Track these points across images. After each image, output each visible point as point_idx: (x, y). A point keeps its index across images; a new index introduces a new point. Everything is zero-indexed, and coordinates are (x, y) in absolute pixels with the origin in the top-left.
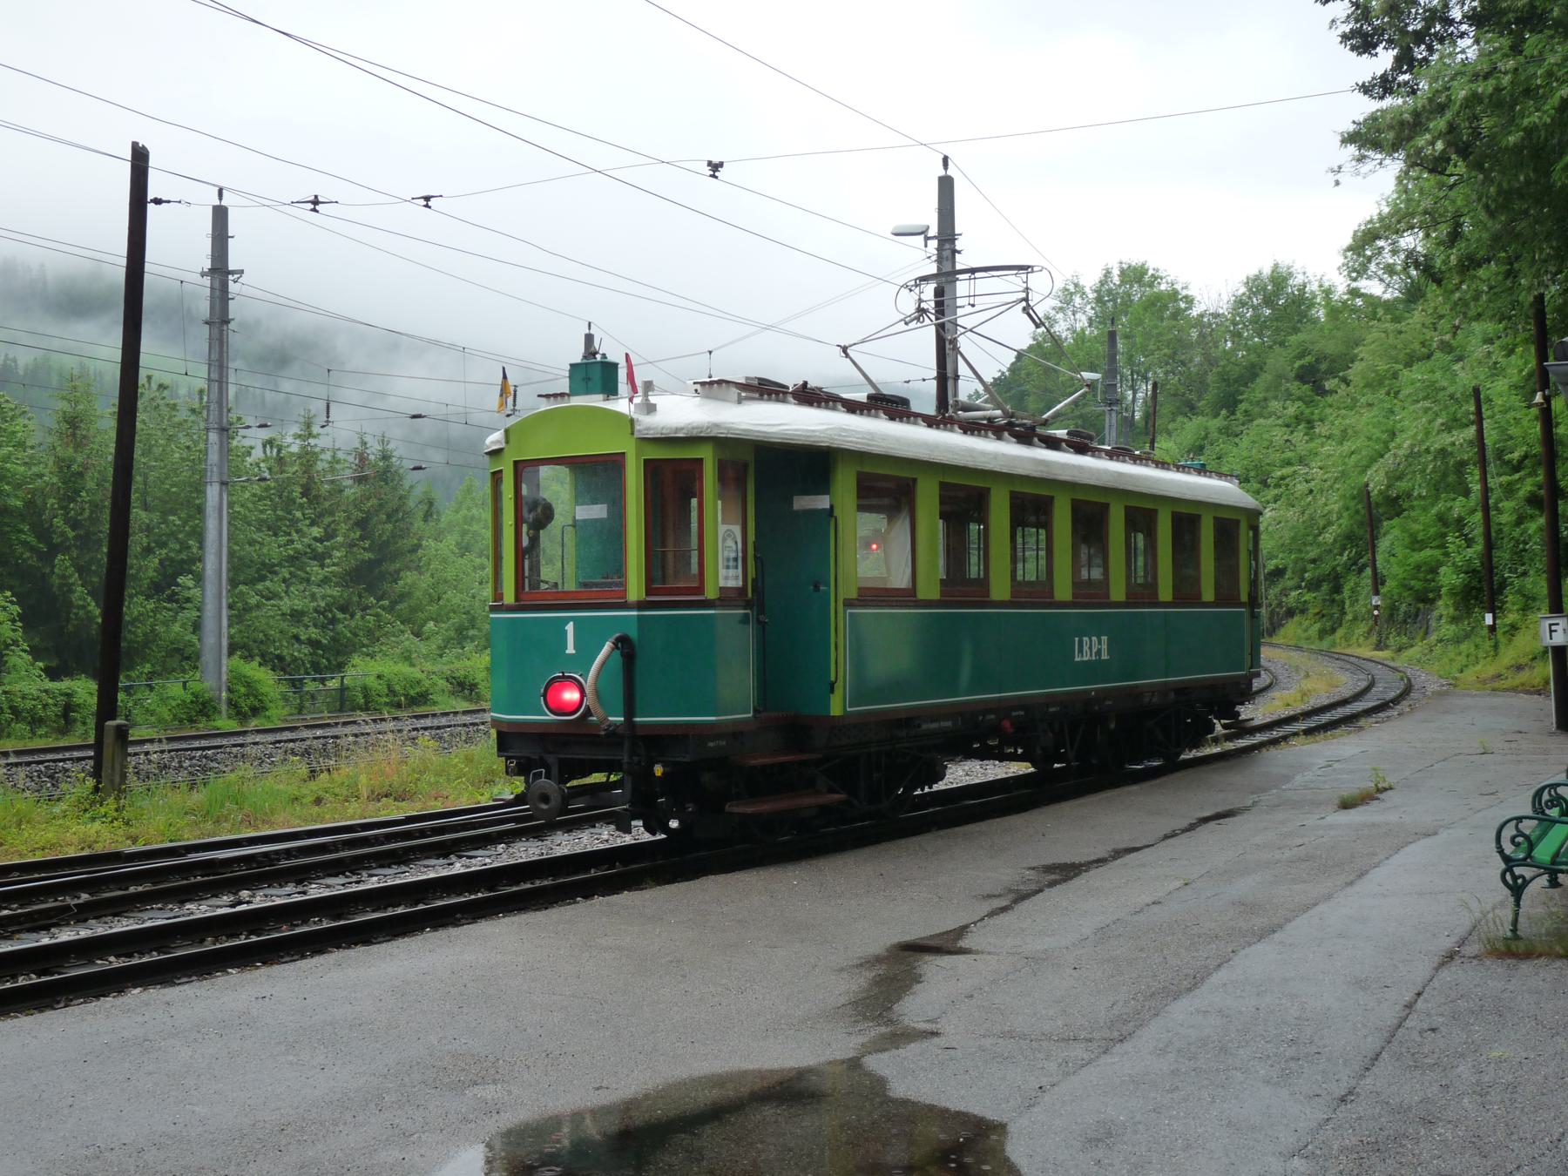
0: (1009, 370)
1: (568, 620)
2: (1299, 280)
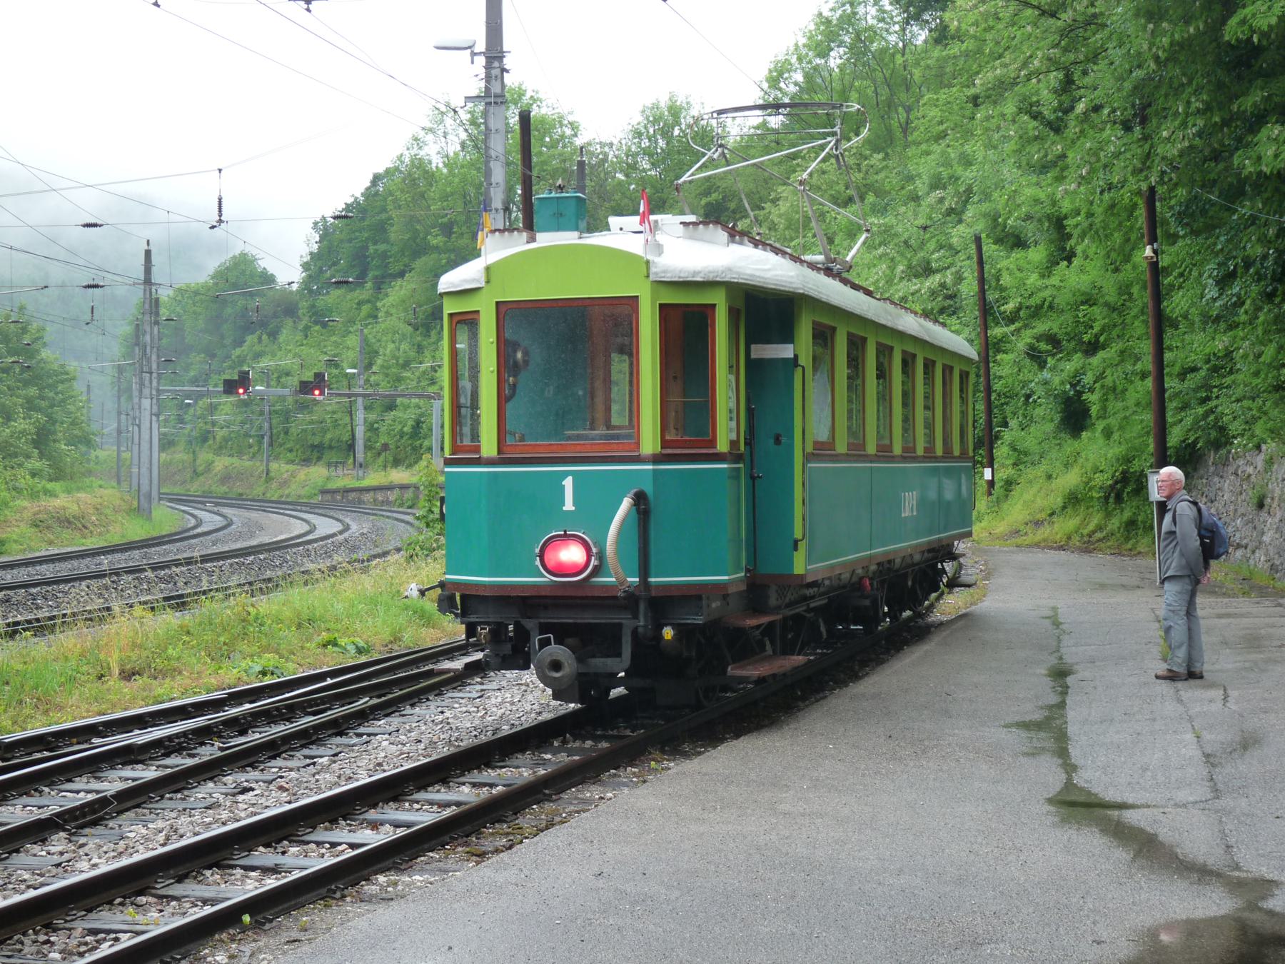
0: (362, 195)
1: (566, 474)
2: (694, 112)
